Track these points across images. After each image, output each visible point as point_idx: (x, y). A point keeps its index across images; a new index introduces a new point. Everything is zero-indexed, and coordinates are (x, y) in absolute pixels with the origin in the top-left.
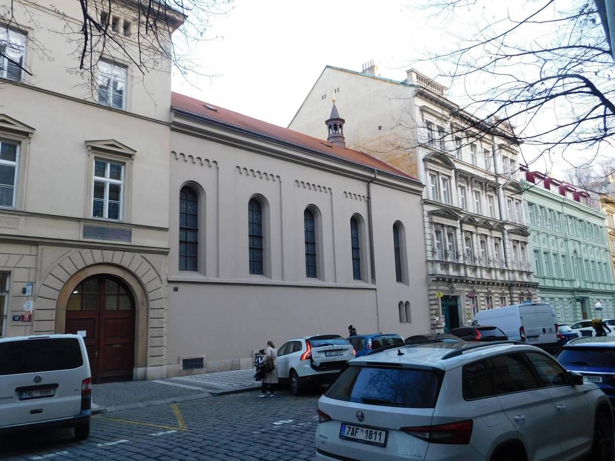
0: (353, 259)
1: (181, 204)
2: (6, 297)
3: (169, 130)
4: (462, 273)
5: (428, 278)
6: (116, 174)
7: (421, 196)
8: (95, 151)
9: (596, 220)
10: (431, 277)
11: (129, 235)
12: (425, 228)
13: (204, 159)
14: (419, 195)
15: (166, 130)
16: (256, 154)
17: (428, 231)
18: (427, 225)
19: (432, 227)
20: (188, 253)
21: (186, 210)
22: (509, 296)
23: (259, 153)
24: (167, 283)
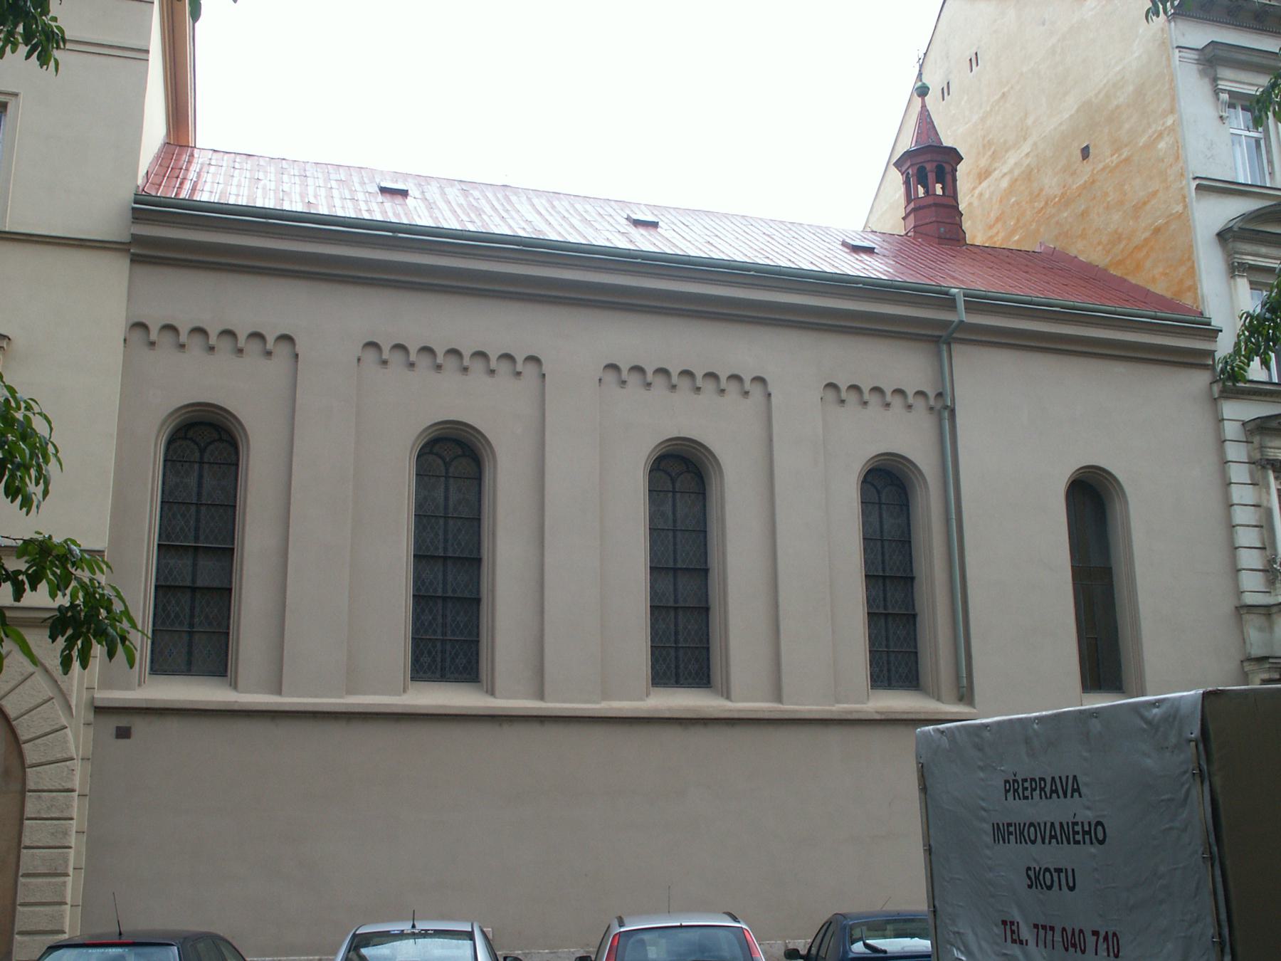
0: (871, 616)
1: (865, 514)
3: (128, 261)
13: (628, 367)
14: (1205, 367)
15: (116, 269)
16: (1119, 368)
18: (1239, 473)
19: (1266, 478)
20: (681, 638)
21: (882, 531)
24: (91, 716)
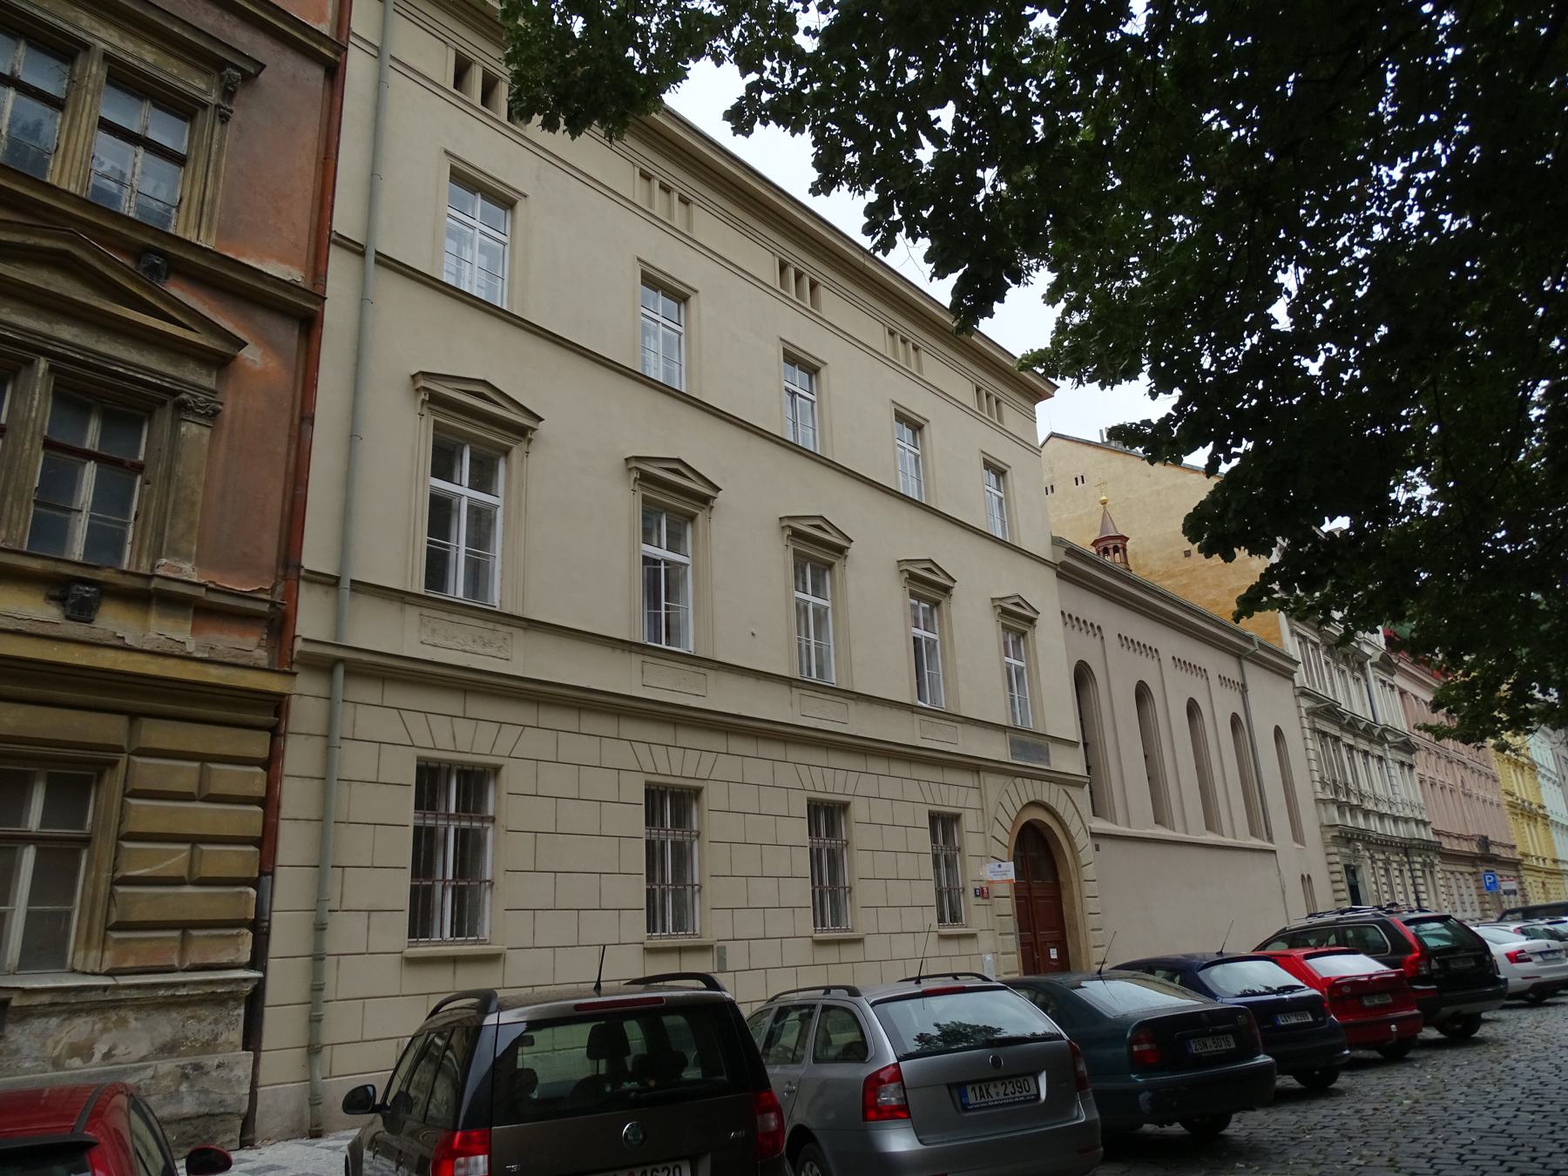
2: (490, 834)
4: (1361, 823)
5: (1322, 833)
6: (483, 480)
7: (1293, 680)
8: (645, 484)
9: (310, 187)
10: (1328, 829)
11: (1044, 755)
12: (1305, 739)
16: (859, 484)
17: (1310, 744)
22: (1407, 866)
23: (944, 519)
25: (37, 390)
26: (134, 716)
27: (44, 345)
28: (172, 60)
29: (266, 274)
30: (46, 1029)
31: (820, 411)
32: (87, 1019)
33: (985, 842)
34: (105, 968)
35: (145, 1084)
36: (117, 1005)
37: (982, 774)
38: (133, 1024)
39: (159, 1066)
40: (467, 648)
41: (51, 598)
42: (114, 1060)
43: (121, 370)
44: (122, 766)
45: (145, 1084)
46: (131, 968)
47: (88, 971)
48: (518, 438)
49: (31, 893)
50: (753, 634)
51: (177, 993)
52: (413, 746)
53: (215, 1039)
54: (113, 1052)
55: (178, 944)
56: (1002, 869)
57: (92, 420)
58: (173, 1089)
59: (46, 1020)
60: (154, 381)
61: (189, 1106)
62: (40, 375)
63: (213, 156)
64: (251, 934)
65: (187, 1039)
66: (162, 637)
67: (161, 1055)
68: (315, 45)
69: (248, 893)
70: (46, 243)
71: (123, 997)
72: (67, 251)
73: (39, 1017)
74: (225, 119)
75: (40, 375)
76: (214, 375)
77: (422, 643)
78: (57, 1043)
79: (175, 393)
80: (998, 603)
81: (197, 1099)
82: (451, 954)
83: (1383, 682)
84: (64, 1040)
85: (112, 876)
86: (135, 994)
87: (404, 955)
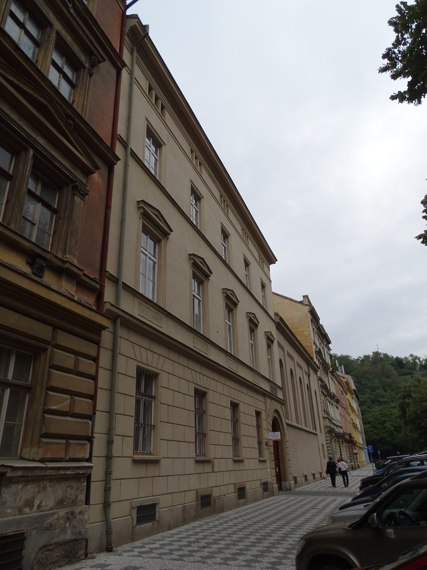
25: (29, 163)
26: (55, 328)
27: (34, 144)
28: (76, 44)
29: (104, 142)
30: (17, 491)
31: (159, 267)
32: (32, 485)
33: (267, 423)
34: (39, 457)
35: (54, 522)
36: (43, 478)
37: (266, 397)
38: (49, 489)
39: (60, 512)
40: (151, 320)
41: (28, 263)
42: (42, 509)
43: (58, 165)
44: (49, 351)
45: (54, 522)
46: (49, 458)
47: (31, 459)
48: (164, 236)
49: (6, 418)
50: (218, 332)
51: (67, 473)
52: (136, 360)
53: (77, 498)
54: (41, 505)
55: (64, 447)
56: (275, 435)
57: (39, 184)
58: (64, 526)
59: (16, 485)
60: (68, 174)
61: (69, 536)
62: (30, 157)
63: (87, 89)
64: (89, 444)
65: (67, 498)
66: (67, 291)
67: (57, 506)
68: (116, 60)
69: (89, 422)
70: (41, 99)
71: (48, 474)
72: (46, 105)
73: (14, 484)
74: (91, 75)
75: (30, 157)
76: (85, 179)
77: (139, 315)
78: (21, 498)
79: (73, 182)
80: (267, 333)
81: (72, 531)
82: (145, 459)
83: (332, 378)
84: (24, 497)
85: (44, 408)
86: (52, 472)
87: (133, 458)
